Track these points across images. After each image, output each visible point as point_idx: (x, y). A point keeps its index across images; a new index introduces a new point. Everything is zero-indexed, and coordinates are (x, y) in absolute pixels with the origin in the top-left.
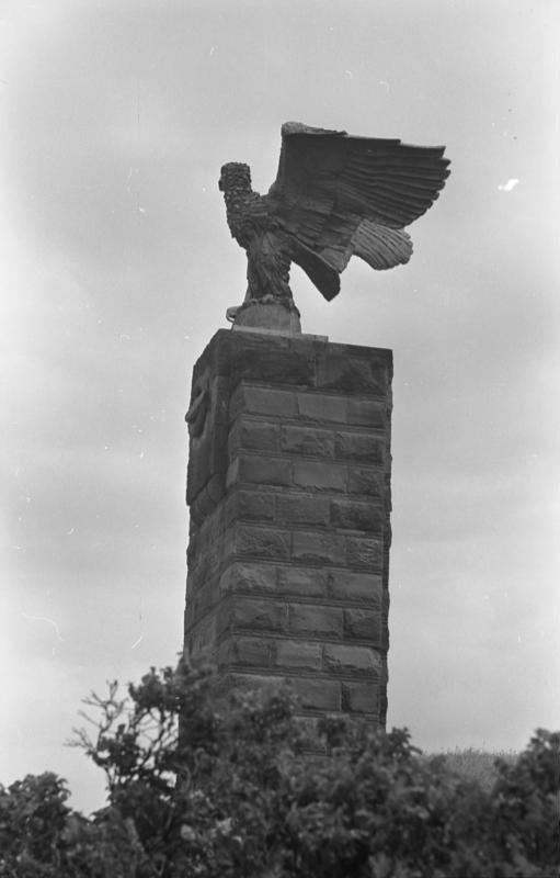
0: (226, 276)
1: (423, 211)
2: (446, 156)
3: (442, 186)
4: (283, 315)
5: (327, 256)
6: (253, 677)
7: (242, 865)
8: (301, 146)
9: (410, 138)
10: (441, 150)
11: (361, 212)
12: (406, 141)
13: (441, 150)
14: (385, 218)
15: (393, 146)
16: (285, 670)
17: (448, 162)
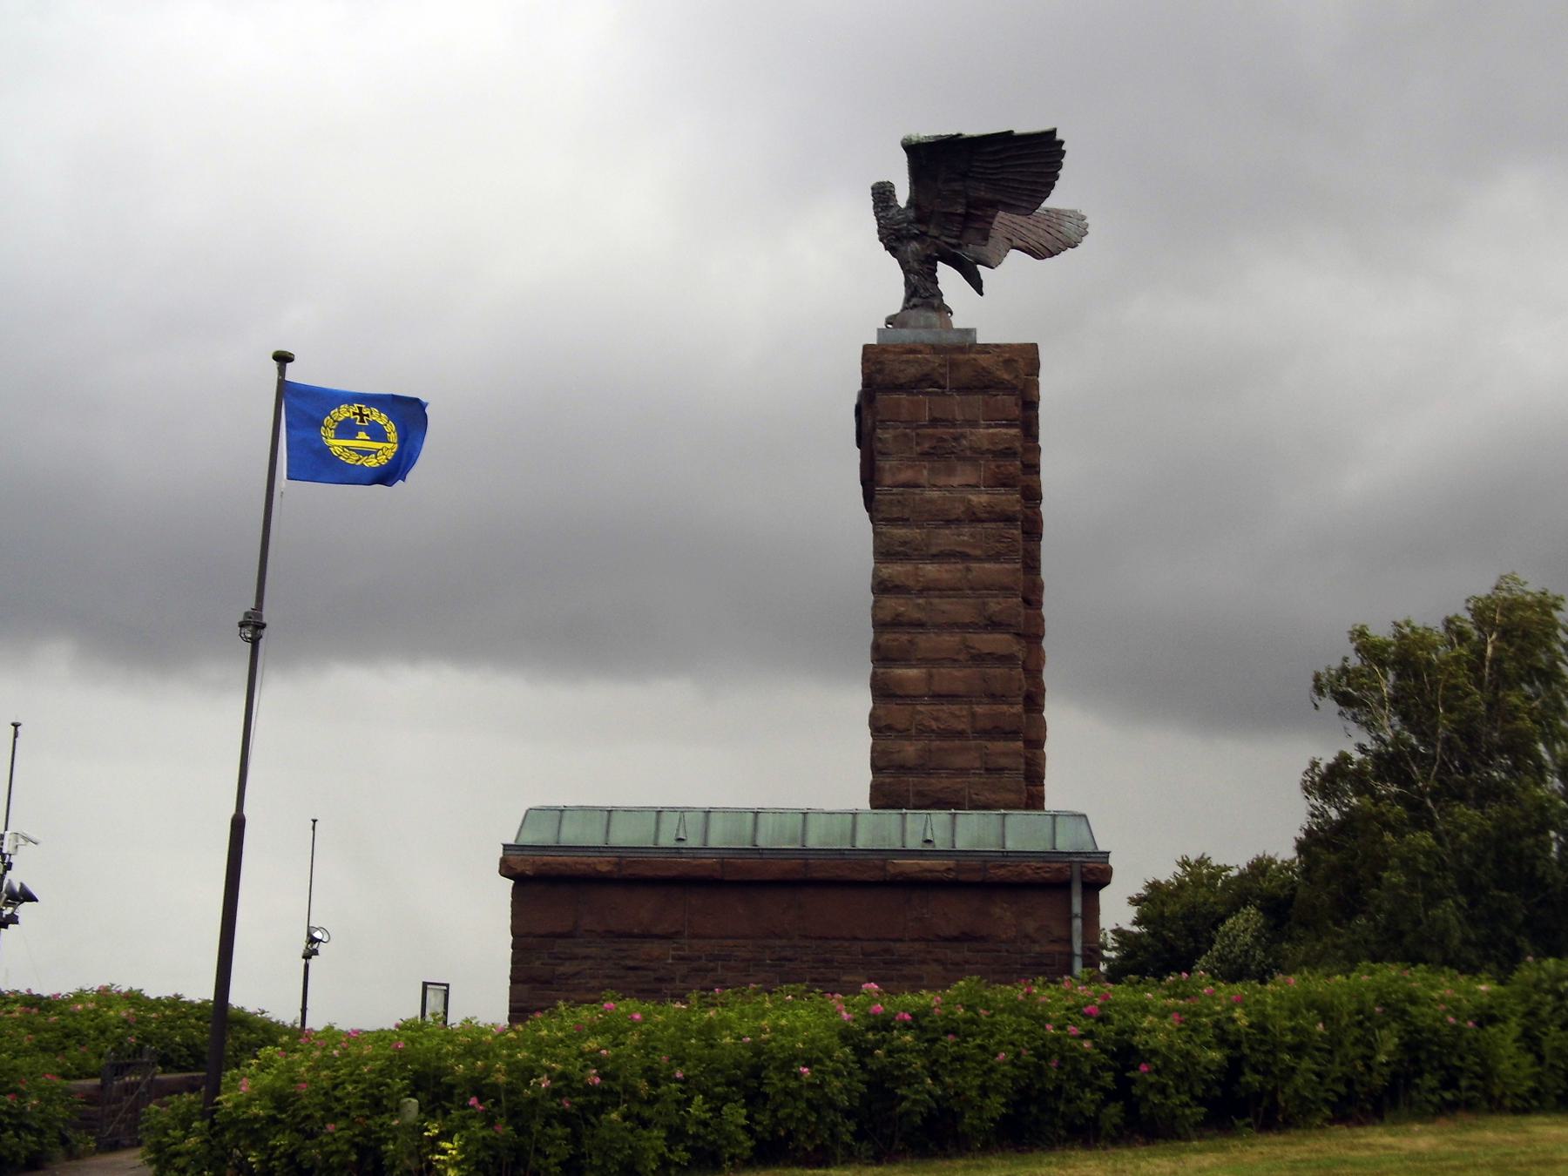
0: (885, 285)
1: (1052, 186)
2: (1059, 137)
3: (1060, 167)
4: (934, 317)
5: (968, 253)
6: (899, 671)
7: (708, 1156)
8: (924, 156)
9: (1021, 127)
10: (1053, 132)
11: (995, 205)
12: (1020, 129)
13: (1053, 132)
14: (912, 351)
15: (1009, 135)
16: (923, 662)
17: (1062, 143)
